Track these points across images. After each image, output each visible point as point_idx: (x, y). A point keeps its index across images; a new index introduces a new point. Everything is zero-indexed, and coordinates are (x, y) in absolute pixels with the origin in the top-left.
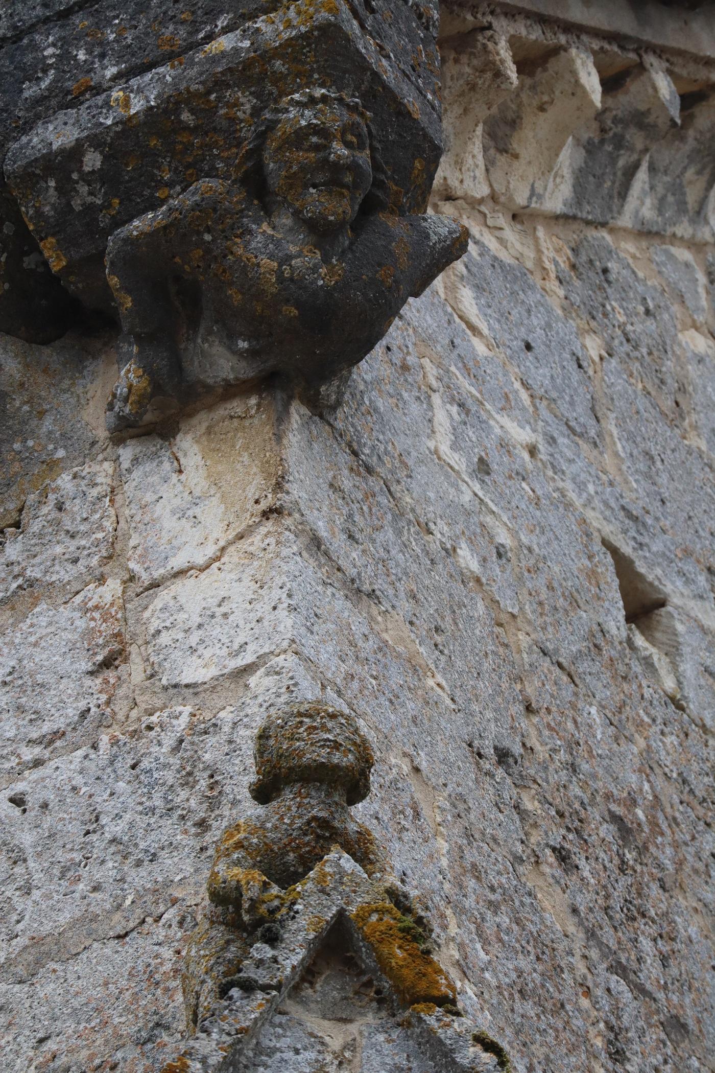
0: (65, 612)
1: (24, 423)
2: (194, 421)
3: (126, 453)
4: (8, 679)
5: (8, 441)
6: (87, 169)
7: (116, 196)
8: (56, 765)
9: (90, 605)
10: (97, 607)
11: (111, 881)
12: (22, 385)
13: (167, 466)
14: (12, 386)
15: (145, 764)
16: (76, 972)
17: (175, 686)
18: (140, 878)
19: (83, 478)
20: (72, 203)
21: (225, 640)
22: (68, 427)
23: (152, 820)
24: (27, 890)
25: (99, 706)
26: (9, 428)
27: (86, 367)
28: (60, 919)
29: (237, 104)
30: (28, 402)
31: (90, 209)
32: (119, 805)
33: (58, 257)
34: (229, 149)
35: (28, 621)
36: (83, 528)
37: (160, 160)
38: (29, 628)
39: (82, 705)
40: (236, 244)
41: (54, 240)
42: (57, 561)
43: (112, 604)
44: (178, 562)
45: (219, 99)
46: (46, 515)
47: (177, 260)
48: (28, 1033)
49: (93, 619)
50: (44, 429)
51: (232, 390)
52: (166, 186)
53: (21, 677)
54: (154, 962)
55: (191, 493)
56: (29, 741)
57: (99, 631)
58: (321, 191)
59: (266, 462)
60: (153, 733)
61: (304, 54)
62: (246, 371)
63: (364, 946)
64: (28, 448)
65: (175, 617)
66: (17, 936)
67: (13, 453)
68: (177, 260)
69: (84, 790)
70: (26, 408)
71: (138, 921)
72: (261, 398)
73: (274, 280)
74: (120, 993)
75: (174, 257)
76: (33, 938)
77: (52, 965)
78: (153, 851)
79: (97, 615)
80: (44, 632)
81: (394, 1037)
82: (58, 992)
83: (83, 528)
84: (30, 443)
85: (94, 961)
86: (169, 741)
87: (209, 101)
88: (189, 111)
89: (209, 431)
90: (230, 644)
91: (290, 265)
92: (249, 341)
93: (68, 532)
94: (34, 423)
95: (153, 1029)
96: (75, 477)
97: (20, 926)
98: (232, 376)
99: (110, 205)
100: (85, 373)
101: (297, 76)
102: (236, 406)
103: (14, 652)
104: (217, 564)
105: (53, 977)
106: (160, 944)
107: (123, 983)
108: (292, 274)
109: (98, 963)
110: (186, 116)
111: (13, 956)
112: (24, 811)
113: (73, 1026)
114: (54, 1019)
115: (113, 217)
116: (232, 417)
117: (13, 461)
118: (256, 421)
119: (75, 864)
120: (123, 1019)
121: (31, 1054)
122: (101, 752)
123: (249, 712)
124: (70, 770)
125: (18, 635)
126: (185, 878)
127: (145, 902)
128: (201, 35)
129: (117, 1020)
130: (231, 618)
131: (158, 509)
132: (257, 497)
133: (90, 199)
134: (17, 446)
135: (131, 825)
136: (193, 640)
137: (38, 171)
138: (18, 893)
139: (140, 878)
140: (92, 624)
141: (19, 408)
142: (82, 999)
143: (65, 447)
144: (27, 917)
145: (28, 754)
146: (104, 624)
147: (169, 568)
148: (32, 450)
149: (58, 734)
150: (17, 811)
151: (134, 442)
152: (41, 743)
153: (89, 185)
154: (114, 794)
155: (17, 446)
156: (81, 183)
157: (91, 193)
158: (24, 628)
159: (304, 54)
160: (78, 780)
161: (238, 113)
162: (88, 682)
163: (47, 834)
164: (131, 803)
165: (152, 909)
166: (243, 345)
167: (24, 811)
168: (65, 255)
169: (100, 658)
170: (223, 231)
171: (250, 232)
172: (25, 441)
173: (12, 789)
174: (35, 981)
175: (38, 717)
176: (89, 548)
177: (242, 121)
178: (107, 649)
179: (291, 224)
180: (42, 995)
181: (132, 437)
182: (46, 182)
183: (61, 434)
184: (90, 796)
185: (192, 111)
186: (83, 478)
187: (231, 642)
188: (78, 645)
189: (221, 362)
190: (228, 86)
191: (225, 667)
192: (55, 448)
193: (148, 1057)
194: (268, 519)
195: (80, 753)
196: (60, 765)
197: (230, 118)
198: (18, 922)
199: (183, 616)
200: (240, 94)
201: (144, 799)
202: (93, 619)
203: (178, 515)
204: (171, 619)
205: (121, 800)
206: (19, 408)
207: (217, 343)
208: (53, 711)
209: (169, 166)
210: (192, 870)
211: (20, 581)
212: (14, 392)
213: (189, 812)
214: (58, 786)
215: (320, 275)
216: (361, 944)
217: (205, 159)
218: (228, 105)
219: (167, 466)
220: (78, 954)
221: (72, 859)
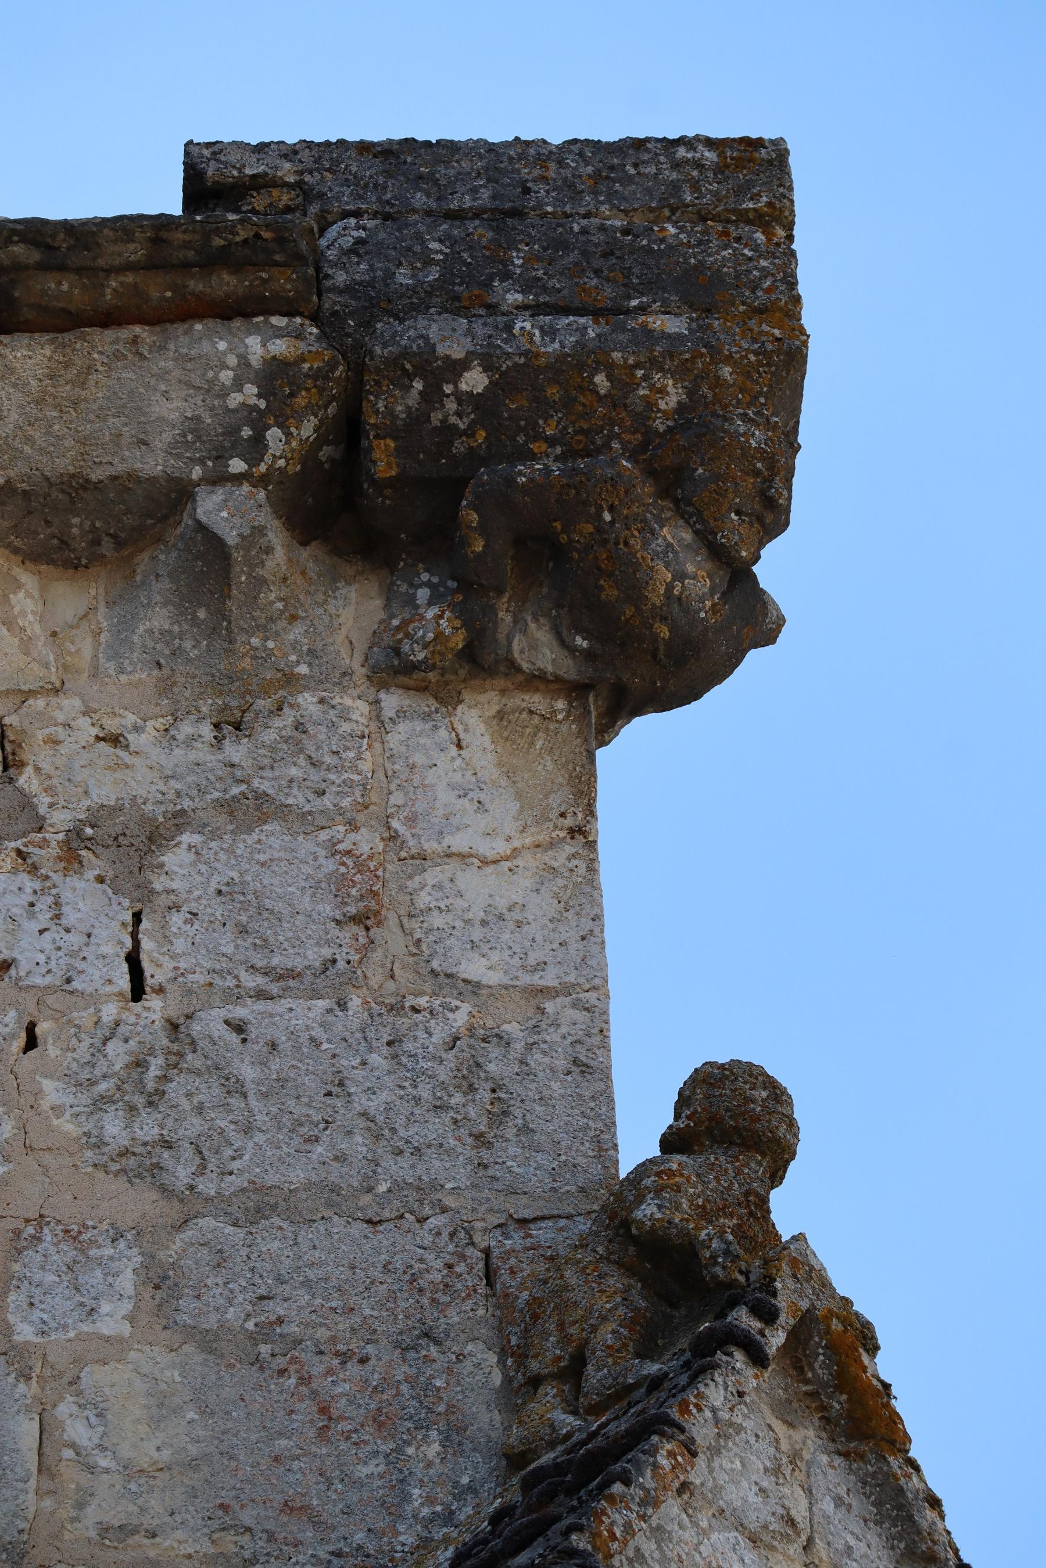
0: (305, 846)
1: (271, 620)
2: (482, 698)
3: (391, 701)
4: (224, 888)
5: (247, 632)
6: (463, 387)
7: (484, 428)
8: (290, 1006)
9: (341, 847)
10: (348, 852)
11: (360, 1157)
12: (285, 579)
13: (443, 733)
14: (274, 576)
15: (409, 1046)
16: (311, 1240)
17: (449, 976)
18: (402, 1168)
19: (333, 707)
20: (432, 415)
21: (517, 948)
22: (319, 645)
23: (417, 1111)
24: (247, 1130)
25: (349, 962)
26: (253, 618)
27: (338, 588)
28: (291, 1174)
29: (663, 391)
30: (283, 600)
31: (448, 431)
32: (373, 1079)
33: (389, 464)
34: (633, 433)
35: (255, 836)
36: (328, 759)
37: (552, 412)
38: (256, 843)
39: (327, 952)
40: (633, 536)
41: (392, 445)
42: (294, 784)
43: (370, 858)
44: (458, 842)
45: (645, 378)
46: (280, 729)
47: (558, 525)
48: (244, 1284)
49: (344, 864)
50: (292, 637)
51: (536, 681)
52: (546, 441)
53: (244, 894)
54: (417, 1266)
55: (475, 774)
56: (252, 967)
57: (353, 881)
58: (743, 521)
59: (577, 777)
60: (418, 1017)
61: (759, 373)
62: (569, 669)
63: (823, 1354)
64: (266, 649)
65: (450, 900)
66: (231, 1173)
67: (248, 647)
68: (558, 525)
69: (325, 1046)
70: (280, 605)
71: (397, 1214)
72: (570, 704)
73: (662, 592)
74: (372, 1283)
75: (555, 521)
76: (254, 1183)
77: (276, 1221)
78: (416, 1144)
79: (350, 862)
80: (276, 855)
81: (836, 1464)
82: (286, 1254)
83: (328, 759)
84: (271, 644)
85: (336, 1237)
86: (440, 1034)
87: (633, 375)
88: (606, 376)
89: (501, 715)
90: (522, 956)
91: (683, 583)
92: (590, 641)
93: (310, 758)
94: (282, 624)
95: (418, 1337)
96: (322, 701)
97: (235, 1165)
98: (550, 669)
99: (473, 435)
100: (337, 594)
101: (741, 391)
102: (537, 701)
103: (233, 862)
104: (508, 864)
105: (279, 1234)
106: (424, 1249)
107: (377, 1273)
108: (681, 593)
109: (340, 1240)
110: (600, 379)
111: (227, 1193)
112: (244, 1041)
113: (306, 1298)
114: (281, 1281)
115: (471, 448)
116: (531, 712)
117: (244, 655)
118: (564, 728)
119: (312, 1123)
120: (375, 1313)
121: (249, 1308)
122: (350, 1013)
123: (548, 1038)
124: (309, 1018)
125: (241, 845)
126: (459, 1188)
127: (406, 1196)
128: (634, 303)
129: (367, 1312)
130: (526, 928)
131: (431, 777)
132: (563, 810)
133: (453, 419)
134: (255, 641)
135: (389, 1107)
136: (477, 933)
137: (408, 366)
138: (232, 1127)
139: (402, 1168)
140: (343, 870)
141: (272, 603)
142: (320, 1273)
143: (310, 665)
144: (246, 1158)
145: (250, 981)
146: (359, 876)
147: (445, 845)
148: (271, 653)
149: (291, 974)
150: (234, 1039)
151: (400, 691)
152: (266, 974)
153: (459, 404)
154: (365, 1064)
155: (255, 641)
156: (452, 398)
157: (459, 414)
158: (249, 841)
159: (759, 373)
160: (318, 1033)
161: (660, 401)
162: (335, 931)
163: (274, 1077)
164: (389, 1081)
165: (415, 1207)
166: (580, 642)
167: (244, 1041)
168: (398, 465)
169: (352, 910)
170: (627, 517)
171: (652, 532)
172: (266, 639)
173: (229, 1011)
174: (254, 1230)
175: (265, 946)
176: (339, 786)
177: (659, 411)
178: (361, 905)
179: (690, 541)
180: (264, 1249)
181: (398, 686)
182: (412, 381)
183: (309, 649)
184: (334, 1056)
185: (609, 377)
186: (333, 707)
187: (526, 954)
188: (323, 885)
189: (537, 645)
190: (661, 369)
191: (516, 978)
192: (298, 662)
193: (411, 1366)
194: (572, 838)
195: (322, 1004)
196: (294, 1007)
197: (648, 402)
198: (233, 1158)
199: (460, 903)
200: (671, 382)
201: (406, 1084)
202: (344, 864)
203: (458, 793)
204: (446, 902)
205: (376, 1074)
206: (272, 603)
207: (547, 628)
208: (286, 945)
209: (558, 423)
210: (468, 1184)
211: (243, 787)
212: (274, 582)
213: (464, 1118)
214: (292, 1029)
215: (704, 607)
216: (821, 1351)
217: (602, 432)
218: (652, 387)
219: (443, 733)
220: (314, 1221)
221: (308, 1115)
